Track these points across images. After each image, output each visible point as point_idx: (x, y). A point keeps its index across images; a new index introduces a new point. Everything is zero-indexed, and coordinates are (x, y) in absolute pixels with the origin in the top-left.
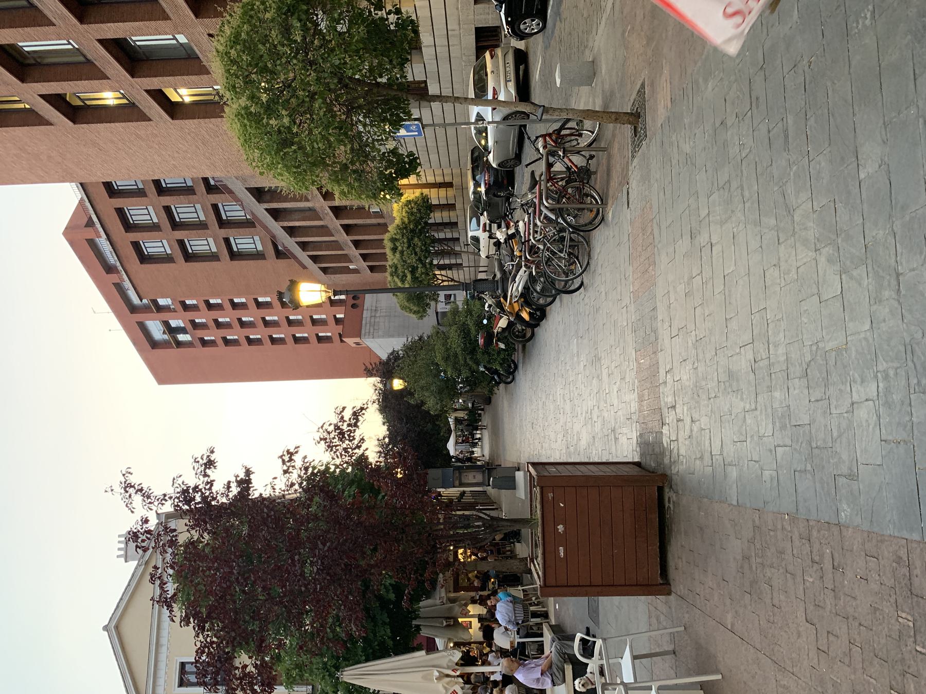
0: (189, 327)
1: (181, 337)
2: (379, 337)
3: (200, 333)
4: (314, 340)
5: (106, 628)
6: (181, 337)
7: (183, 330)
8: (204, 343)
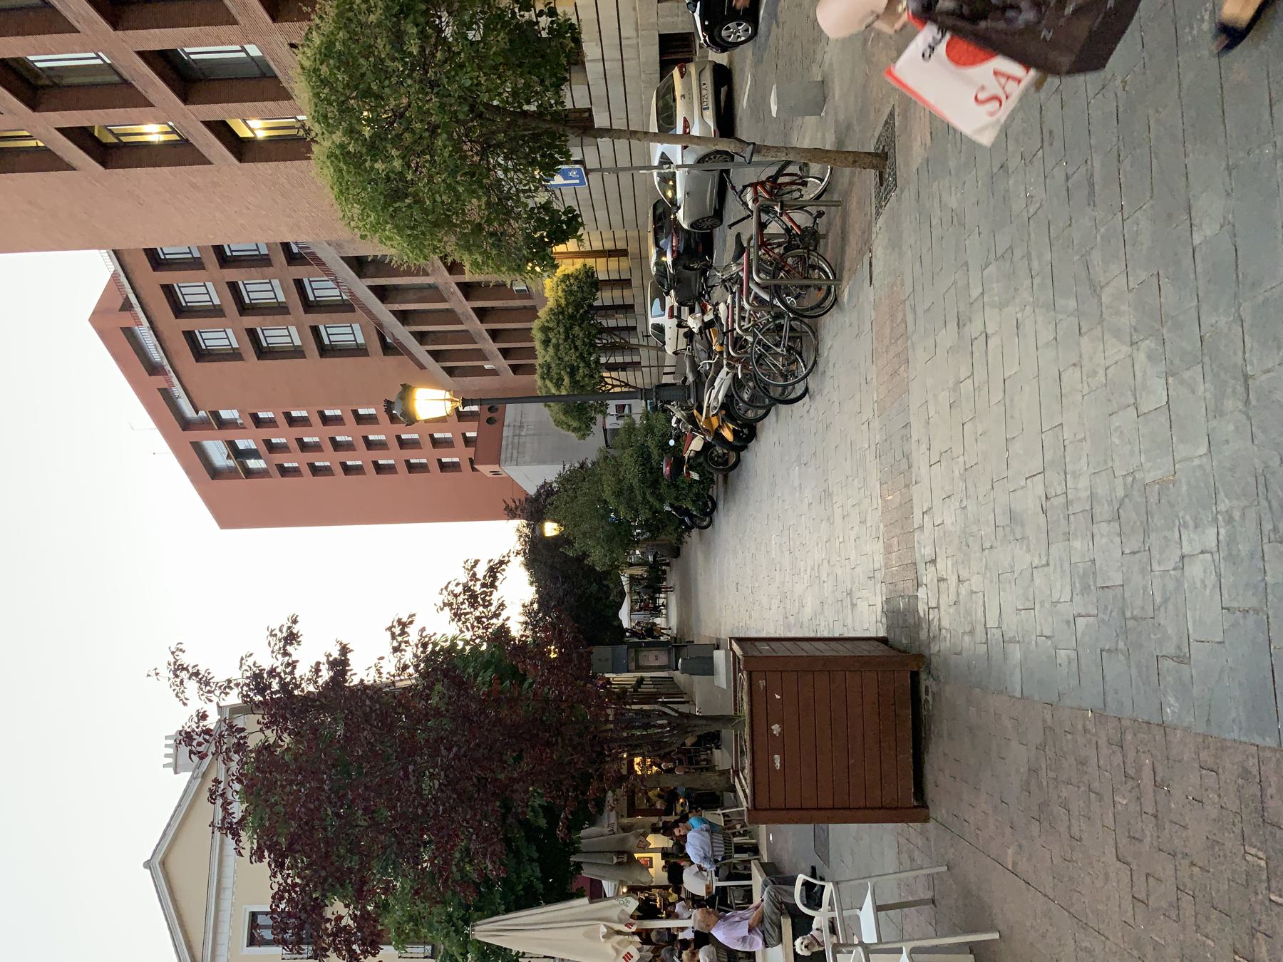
0: (263, 449)
1: (253, 464)
2: (525, 463)
3: (278, 458)
4: (435, 467)
5: (148, 865)
6: (253, 464)
7: (254, 454)
8: (284, 471)
